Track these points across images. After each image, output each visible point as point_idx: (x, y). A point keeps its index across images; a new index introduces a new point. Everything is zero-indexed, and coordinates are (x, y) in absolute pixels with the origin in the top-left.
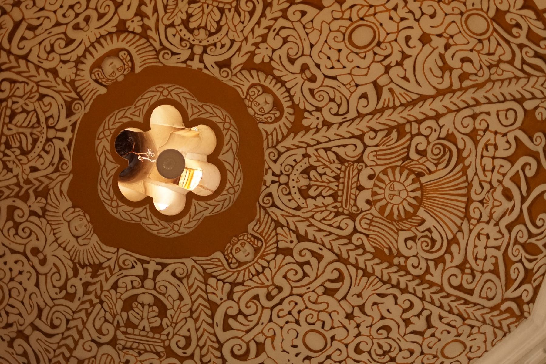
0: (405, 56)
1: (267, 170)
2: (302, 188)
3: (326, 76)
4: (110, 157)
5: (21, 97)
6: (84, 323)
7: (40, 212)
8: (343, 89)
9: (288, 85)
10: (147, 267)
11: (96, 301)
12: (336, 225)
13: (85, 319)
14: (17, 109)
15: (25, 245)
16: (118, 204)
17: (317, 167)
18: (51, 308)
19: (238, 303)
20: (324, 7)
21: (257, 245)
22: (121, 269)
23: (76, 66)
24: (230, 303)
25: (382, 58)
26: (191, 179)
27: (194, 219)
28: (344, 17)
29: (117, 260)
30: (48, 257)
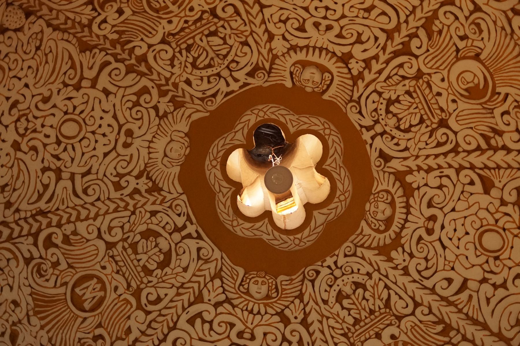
0: (504, 285)
1: (335, 255)
2: (343, 292)
3: (440, 239)
4: (246, 131)
5: (232, 29)
6: (107, 213)
7: (161, 113)
8: (441, 261)
9: (410, 217)
10: (188, 226)
11: (131, 208)
12: (336, 340)
13: (111, 210)
14: (221, 33)
15: (128, 122)
16: (216, 166)
17: (367, 290)
18: (98, 179)
19: (217, 315)
20: (489, 194)
21: (272, 294)
22: (170, 207)
23: (289, 49)
24: (212, 309)
25: (489, 270)
26: (289, 208)
27: (252, 231)
28: (495, 215)
29: (175, 199)
30: (133, 146)
